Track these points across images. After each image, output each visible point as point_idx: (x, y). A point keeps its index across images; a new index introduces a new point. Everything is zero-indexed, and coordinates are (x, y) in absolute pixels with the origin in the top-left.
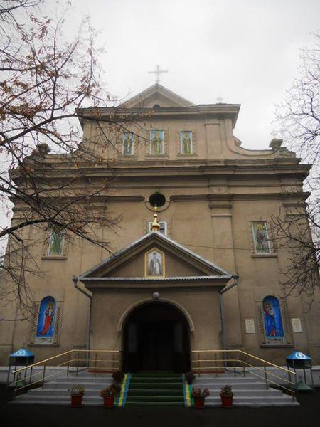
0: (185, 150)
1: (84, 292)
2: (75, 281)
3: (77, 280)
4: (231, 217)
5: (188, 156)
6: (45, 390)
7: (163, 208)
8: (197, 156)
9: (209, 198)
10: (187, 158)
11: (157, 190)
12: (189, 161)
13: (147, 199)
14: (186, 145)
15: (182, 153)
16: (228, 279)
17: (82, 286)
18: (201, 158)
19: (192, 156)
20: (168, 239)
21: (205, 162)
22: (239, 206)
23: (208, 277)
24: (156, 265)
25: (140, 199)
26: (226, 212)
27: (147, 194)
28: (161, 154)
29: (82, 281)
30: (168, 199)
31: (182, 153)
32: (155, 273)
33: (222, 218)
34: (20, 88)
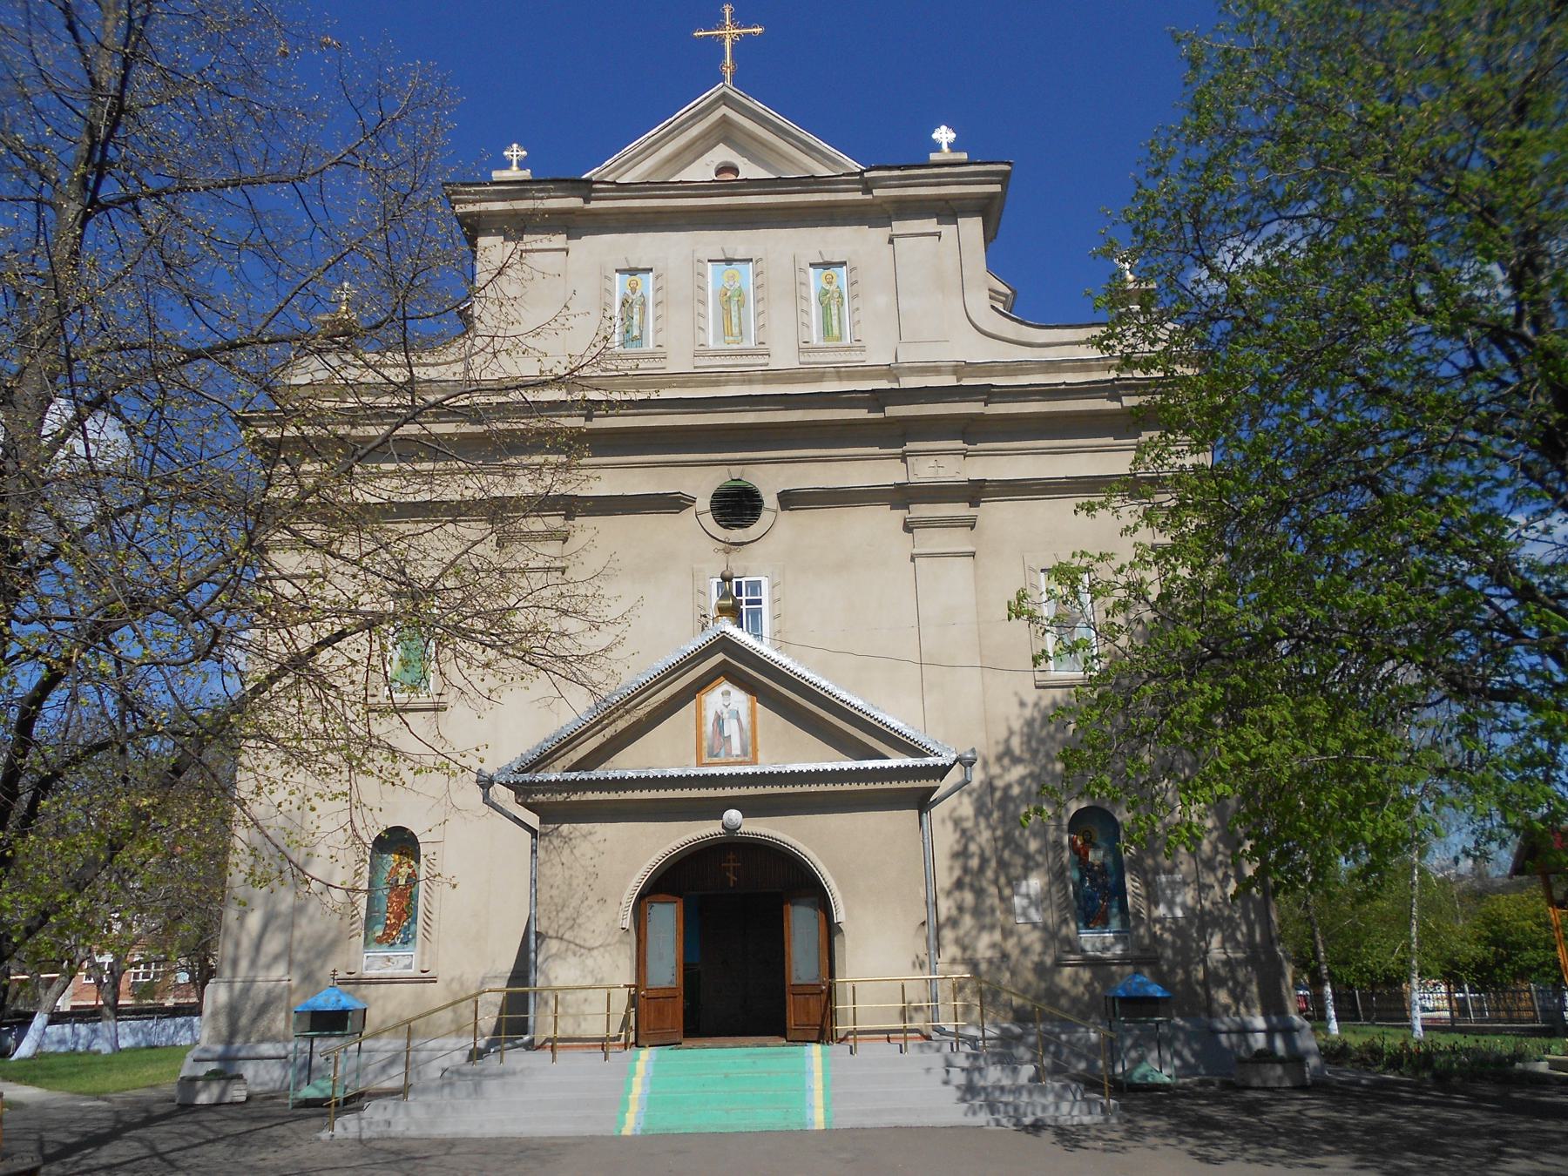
0: (826, 330)
1: (516, 820)
2: (486, 783)
3: (491, 782)
4: (973, 555)
5: (837, 349)
6: (594, 205)
7: (755, 530)
8: (862, 349)
9: (901, 496)
10: (830, 357)
11: (736, 471)
12: (840, 373)
13: (703, 503)
14: (826, 309)
15: (816, 338)
16: (941, 772)
17: (503, 795)
18: (879, 356)
19: (849, 349)
20: (775, 655)
21: (891, 371)
22: (994, 513)
23: (886, 764)
24: (731, 728)
25: (674, 503)
26: (957, 540)
27: (701, 481)
28: (745, 345)
29: (508, 785)
30: (770, 501)
31: (816, 338)
32: (729, 754)
33: (1004, 335)
34: (180, 522)
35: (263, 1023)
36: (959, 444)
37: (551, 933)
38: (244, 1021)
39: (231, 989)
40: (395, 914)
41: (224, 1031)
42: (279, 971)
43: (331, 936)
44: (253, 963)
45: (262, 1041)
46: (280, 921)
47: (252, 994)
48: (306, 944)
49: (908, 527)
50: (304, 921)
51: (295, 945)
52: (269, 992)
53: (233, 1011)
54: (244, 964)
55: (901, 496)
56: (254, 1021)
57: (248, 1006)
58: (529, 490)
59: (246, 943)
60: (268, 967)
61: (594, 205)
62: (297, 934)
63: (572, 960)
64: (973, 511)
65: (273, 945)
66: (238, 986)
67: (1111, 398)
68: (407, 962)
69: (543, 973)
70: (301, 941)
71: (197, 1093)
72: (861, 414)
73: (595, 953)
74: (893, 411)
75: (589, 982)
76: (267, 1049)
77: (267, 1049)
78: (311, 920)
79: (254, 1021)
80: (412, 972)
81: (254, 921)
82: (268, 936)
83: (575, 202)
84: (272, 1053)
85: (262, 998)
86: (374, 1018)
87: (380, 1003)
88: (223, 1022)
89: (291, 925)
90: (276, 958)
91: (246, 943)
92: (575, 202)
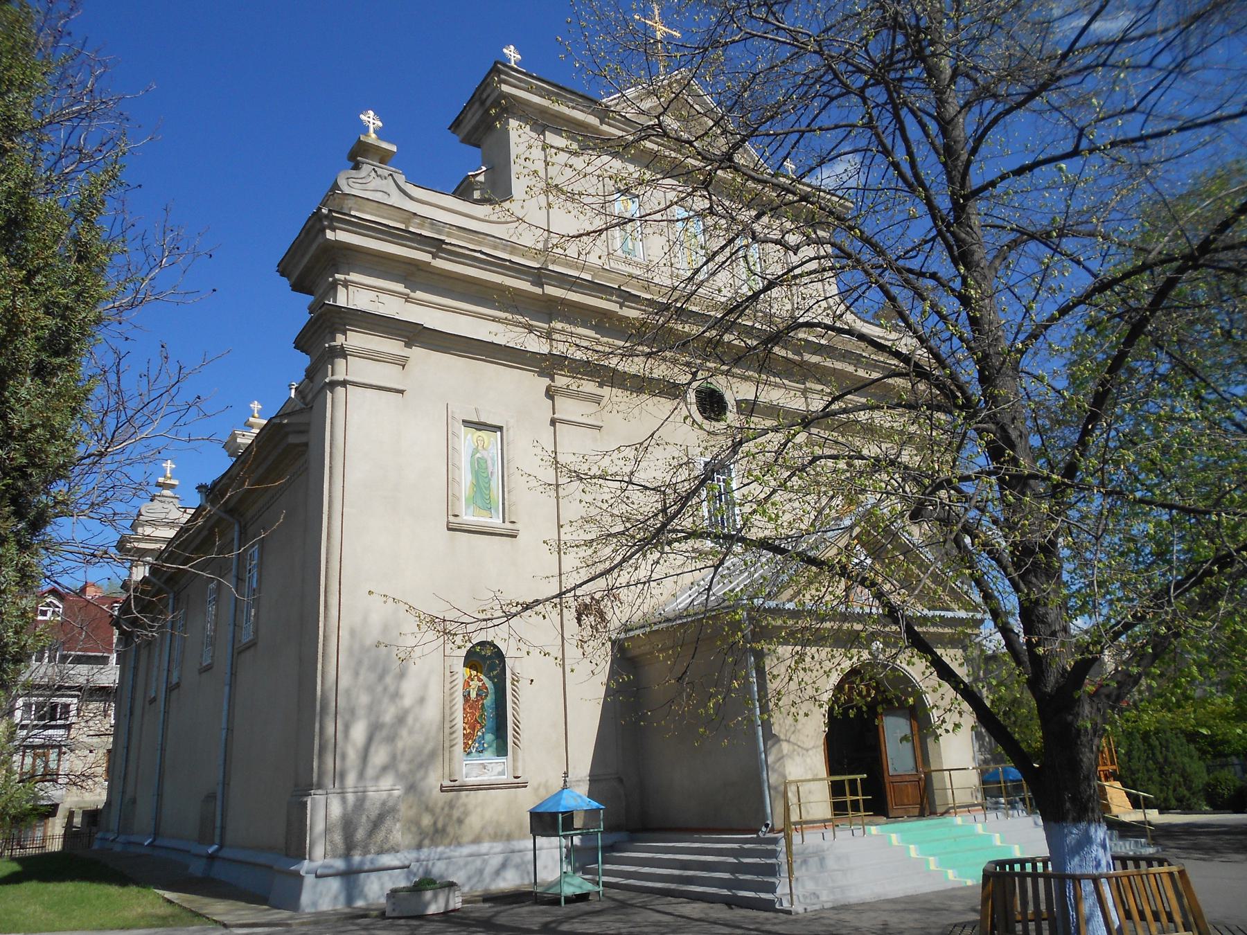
6: (605, 128)
23: (949, 614)
35: (381, 835)
36: (399, 287)
37: (782, 737)
38: (360, 834)
39: (344, 801)
40: (493, 723)
41: (341, 846)
42: (387, 782)
43: (429, 747)
44: (361, 775)
45: (381, 852)
46: (384, 733)
47: (367, 804)
48: (408, 755)
49: (550, 394)
50: (404, 732)
51: (399, 757)
52: (384, 804)
53: (348, 826)
54: (351, 779)
55: (547, 365)
56: (371, 832)
57: (364, 819)
58: (1013, 437)
59: (352, 755)
60: (377, 778)
61: (605, 128)
62: (400, 744)
63: (798, 759)
64: (406, 352)
65: (379, 756)
66: (351, 798)
67: (533, 284)
68: (500, 768)
69: (774, 770)
70: (403, 753)
71: (427, 905)
72: (525, 285)
73: (811, 752)
74: (551, 290)
75: (809, 777)
76: (387, 860)
77: (387, 860)
78: (411, 732)
79: (371, 832)
80: (504, 779)
81: (359, 732)
82: (373, 749)
83: (593, 120)
84: (396, 863)
85: (374, 813)
86: (474, 822)
87: (479, 810)
88: (338, 838)
89: (391, 739)
90: (385, 769)
91: (352, 755)
92: (593, 120)
